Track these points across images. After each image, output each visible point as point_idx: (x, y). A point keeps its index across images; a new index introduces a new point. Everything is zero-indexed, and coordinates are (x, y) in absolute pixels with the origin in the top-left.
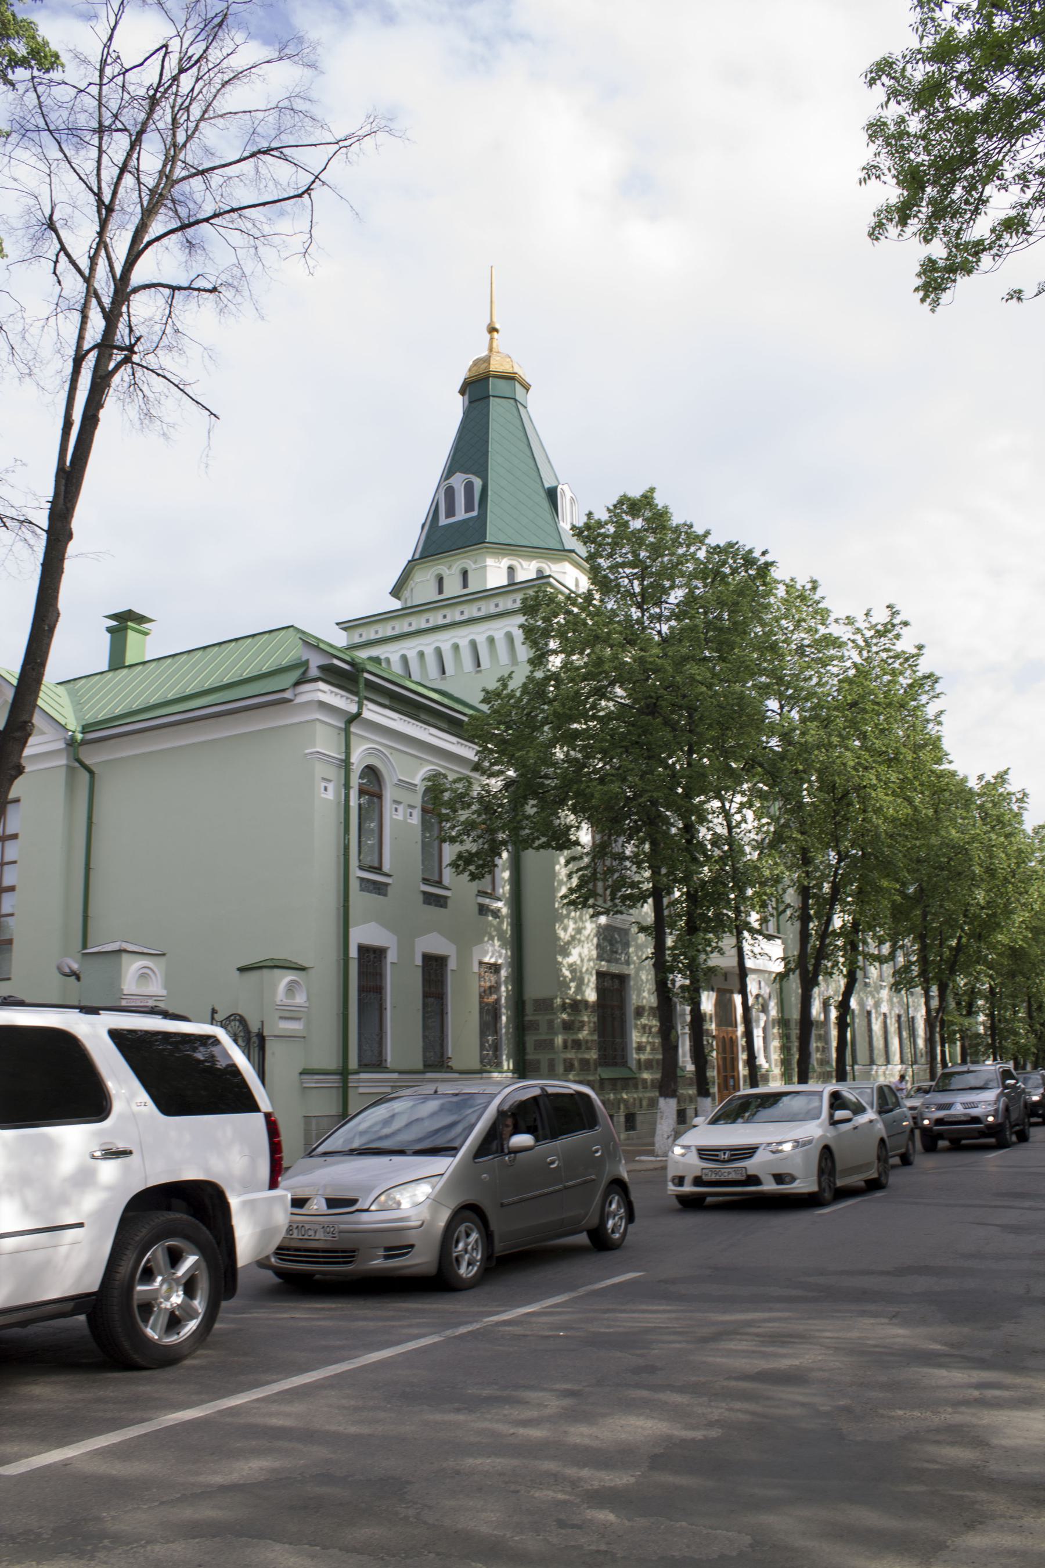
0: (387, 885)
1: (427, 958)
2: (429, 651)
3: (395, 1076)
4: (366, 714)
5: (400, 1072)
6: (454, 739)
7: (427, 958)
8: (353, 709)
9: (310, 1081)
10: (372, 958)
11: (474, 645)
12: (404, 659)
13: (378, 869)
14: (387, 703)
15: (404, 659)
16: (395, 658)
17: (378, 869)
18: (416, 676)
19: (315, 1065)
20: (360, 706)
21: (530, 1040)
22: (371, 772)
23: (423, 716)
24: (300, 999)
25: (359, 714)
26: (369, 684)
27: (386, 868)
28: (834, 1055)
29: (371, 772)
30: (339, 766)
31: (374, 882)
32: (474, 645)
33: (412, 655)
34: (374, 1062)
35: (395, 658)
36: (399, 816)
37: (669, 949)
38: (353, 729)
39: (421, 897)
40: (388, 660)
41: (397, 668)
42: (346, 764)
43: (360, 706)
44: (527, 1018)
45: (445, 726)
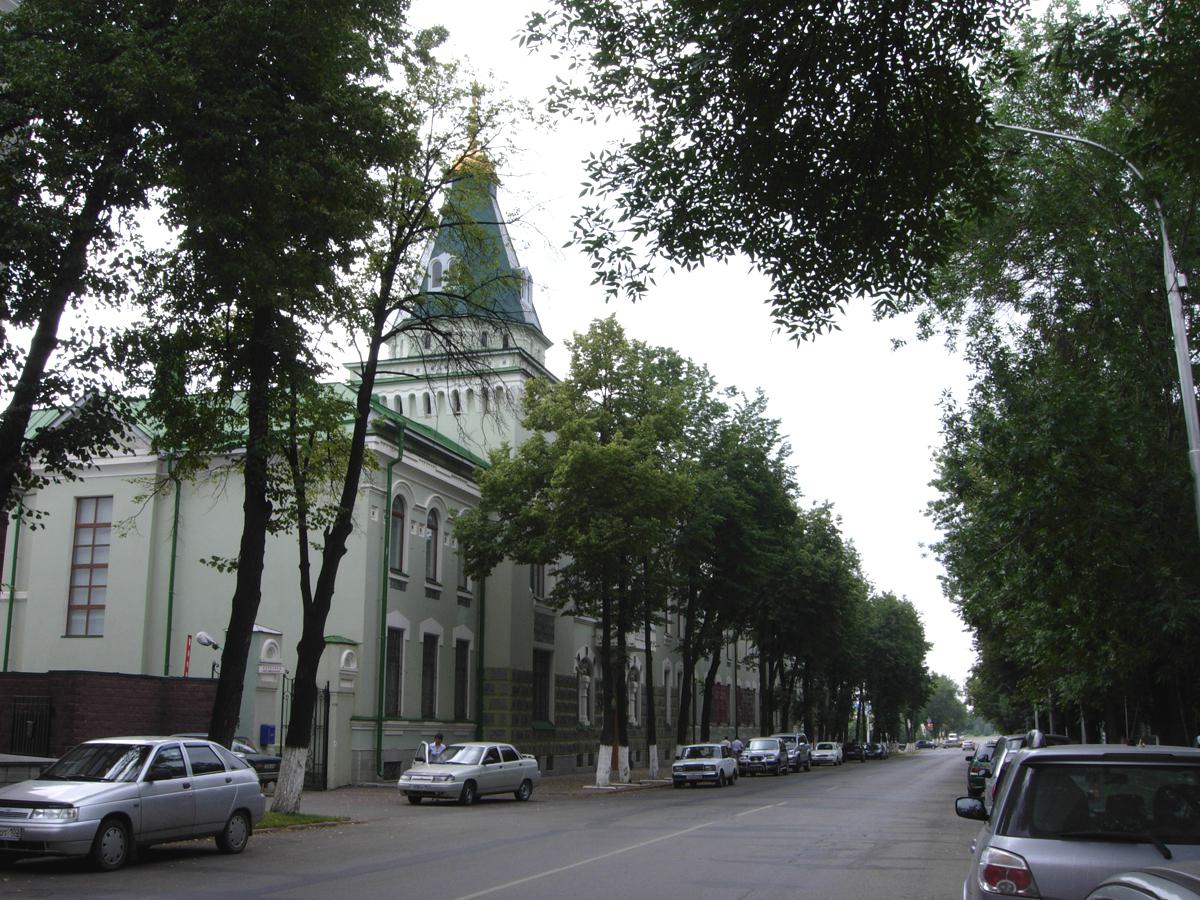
0: (406, 583)
1: (459, 641)
2: (419, 395)
3: (407, 723)
4: (404, 460)
5: (410, 721)
6: (449, 473)
7: (459, 641)
8: (396, 455)
9: (358, 725)
10: (396, 633)
11: (456, 395)
12: (398, 400)
13: (399, 571)
14: (411, 447)
15: (398, 400)
16: (391, 397)
17: (399, 571)
18: (406, 413)
19: (360, 714)
20: (401, 454)
21: (487, 700)
22: (399, 498)
23: (463, 472)
24: (353, 666)
25: (399, 460)
26: (408, 438)
27: (405, 570)
28: (998, 773)
29: (399, 498)
30: (383, 497)
31: (399, 581)
32: (456, 395)
33: (405, 396)
34: (394, 714)
35: (391, 397)
36: (414, 532)
37: (26, 440)
38: (394, 470)
39: (424, 591)
40: (385, 398)
41: (391, 405)
42: (388, 493)
43: (401, 454)
44: (485, 683)
45: (441, 461)
